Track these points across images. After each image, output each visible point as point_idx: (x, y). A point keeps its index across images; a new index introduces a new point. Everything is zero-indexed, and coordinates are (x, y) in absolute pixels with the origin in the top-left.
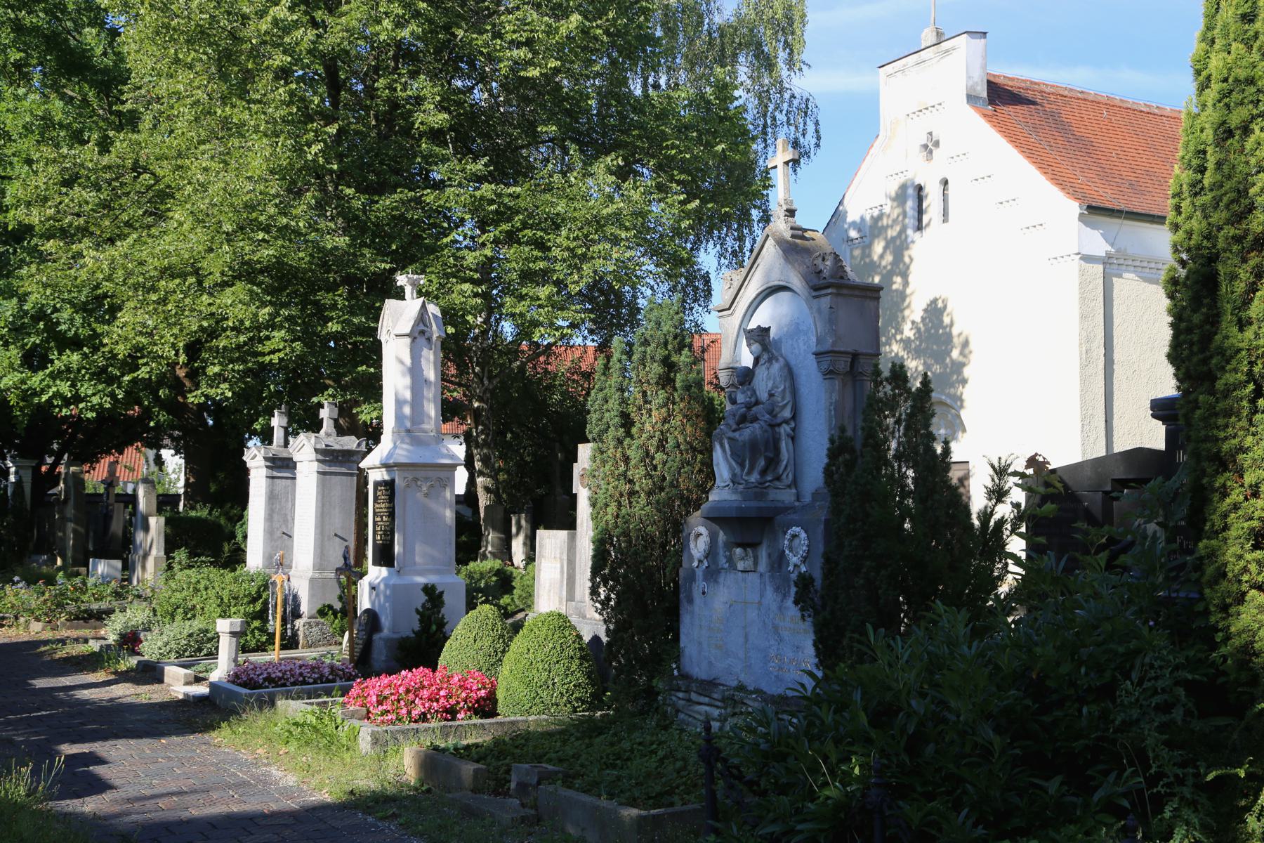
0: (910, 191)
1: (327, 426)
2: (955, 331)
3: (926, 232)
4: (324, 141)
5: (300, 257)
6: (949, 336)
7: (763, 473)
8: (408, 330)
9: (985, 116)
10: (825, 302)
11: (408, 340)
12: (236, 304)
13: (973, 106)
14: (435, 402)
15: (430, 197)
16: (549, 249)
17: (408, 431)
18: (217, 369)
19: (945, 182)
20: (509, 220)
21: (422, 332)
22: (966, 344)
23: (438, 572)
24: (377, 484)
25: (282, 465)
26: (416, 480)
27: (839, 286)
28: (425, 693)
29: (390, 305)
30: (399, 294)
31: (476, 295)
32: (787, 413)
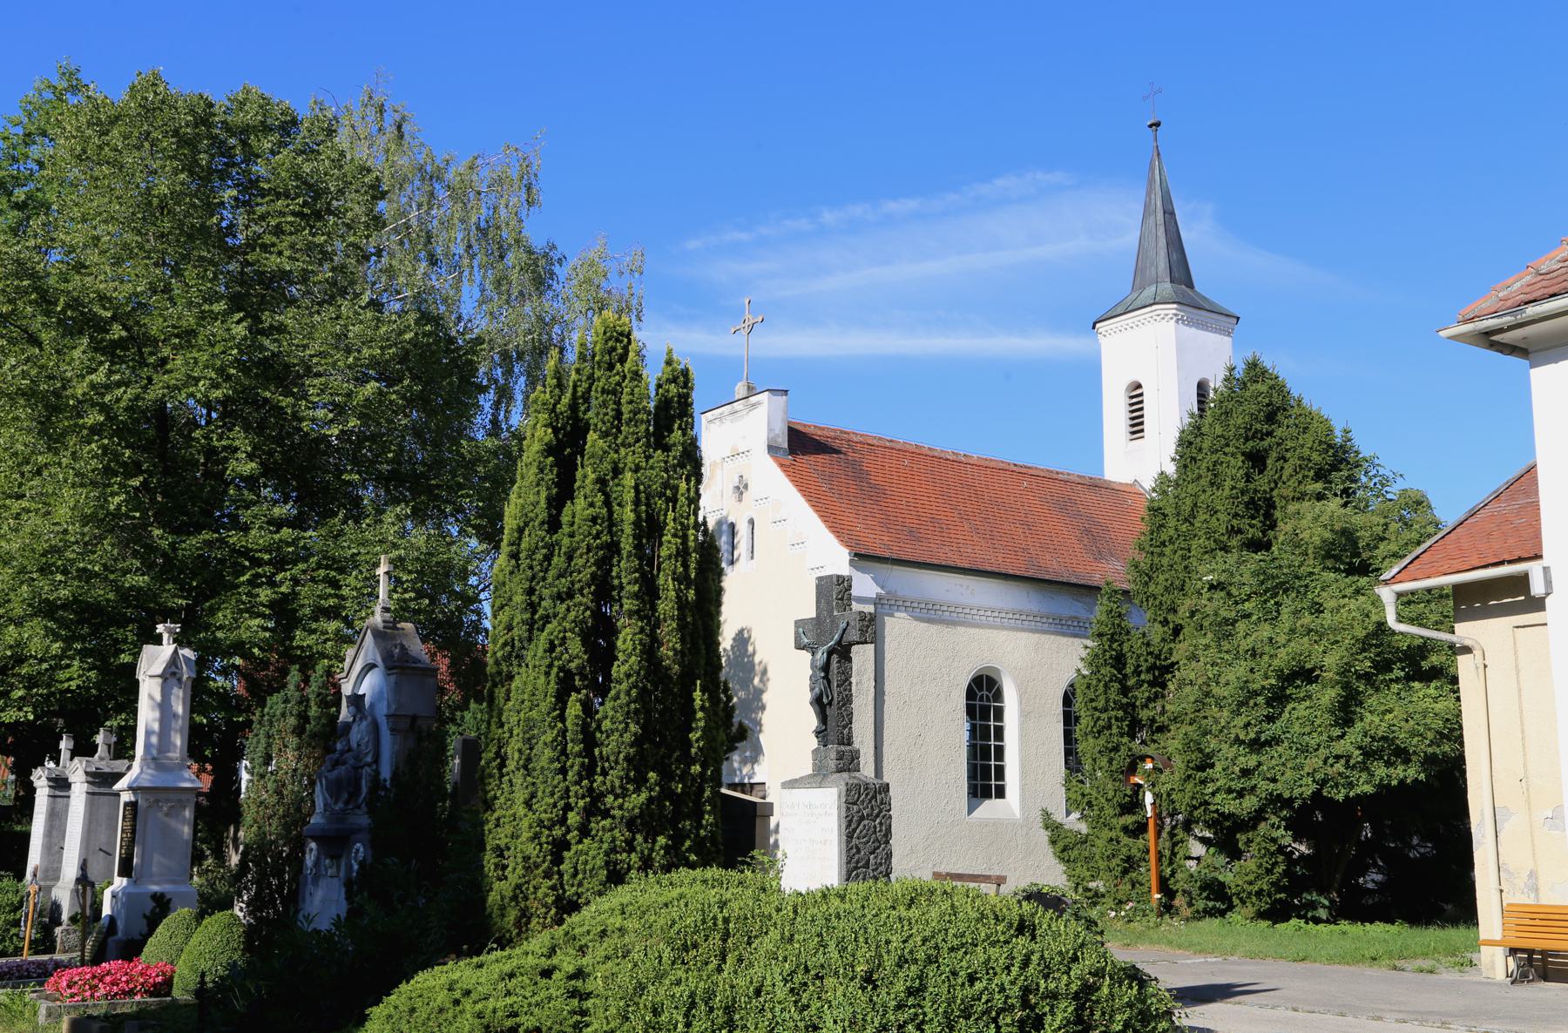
0: (725, 527)
1: (102, 750)
2: (757, 660)
3: (737, 566)
4: (127, 493)
5: (101, 593)
6: (753, 665)
7: (347, 803)
8: (159, 671)
9: (781, 465)
10: (393, 678)
11: (160, 680)
12: (36, 638)
13: (775, 458)
14: (181, 731)
15: (234, 538)
16: (340, 588)
17: (154, 759)
18: (20, 693)
19: (752, 522)
20: (305, 560)
21: (174, 674)
22: (765, 672)
23: (173, 882)
24: (126, 804)
25: (61, 784)
26: (157, 801)
27: (403, 668)
28: (108, 979)
29: (148, 649)
30: (158, 640)
31: (265, 629)
32: (369, 759)
